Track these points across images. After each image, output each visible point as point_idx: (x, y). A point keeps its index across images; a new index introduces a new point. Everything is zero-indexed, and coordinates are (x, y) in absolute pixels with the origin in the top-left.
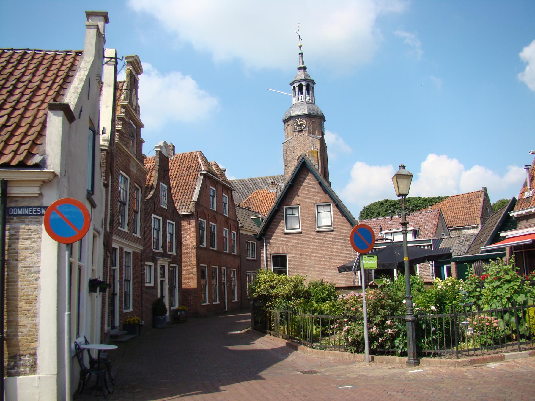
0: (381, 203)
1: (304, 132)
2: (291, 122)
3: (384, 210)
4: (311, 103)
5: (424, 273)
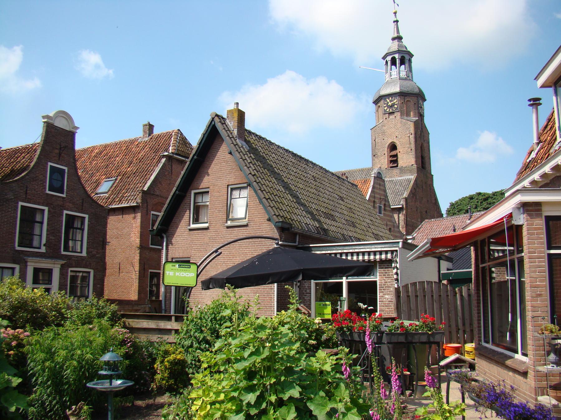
0: (471, 198)
1: (396, 114)
2: (382, 103)
3: (474, 206)
4: (409, 77)
5: (387, 296)
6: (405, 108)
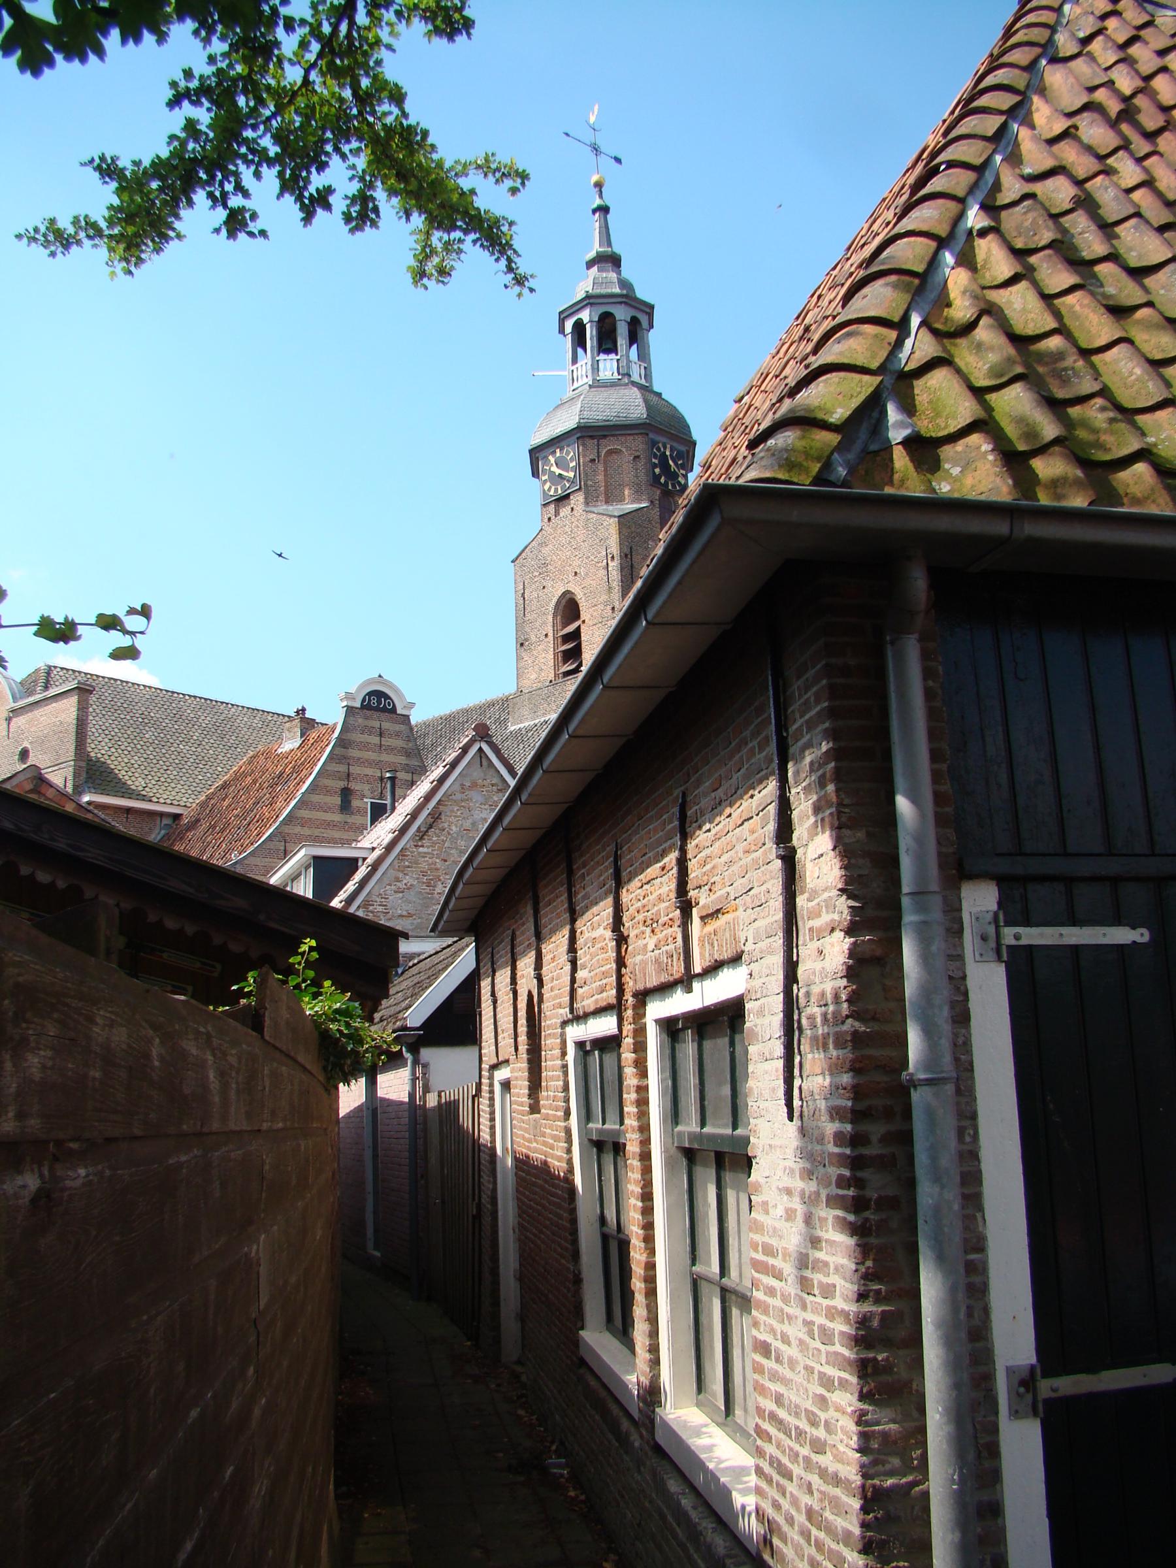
6: (601, 477)
